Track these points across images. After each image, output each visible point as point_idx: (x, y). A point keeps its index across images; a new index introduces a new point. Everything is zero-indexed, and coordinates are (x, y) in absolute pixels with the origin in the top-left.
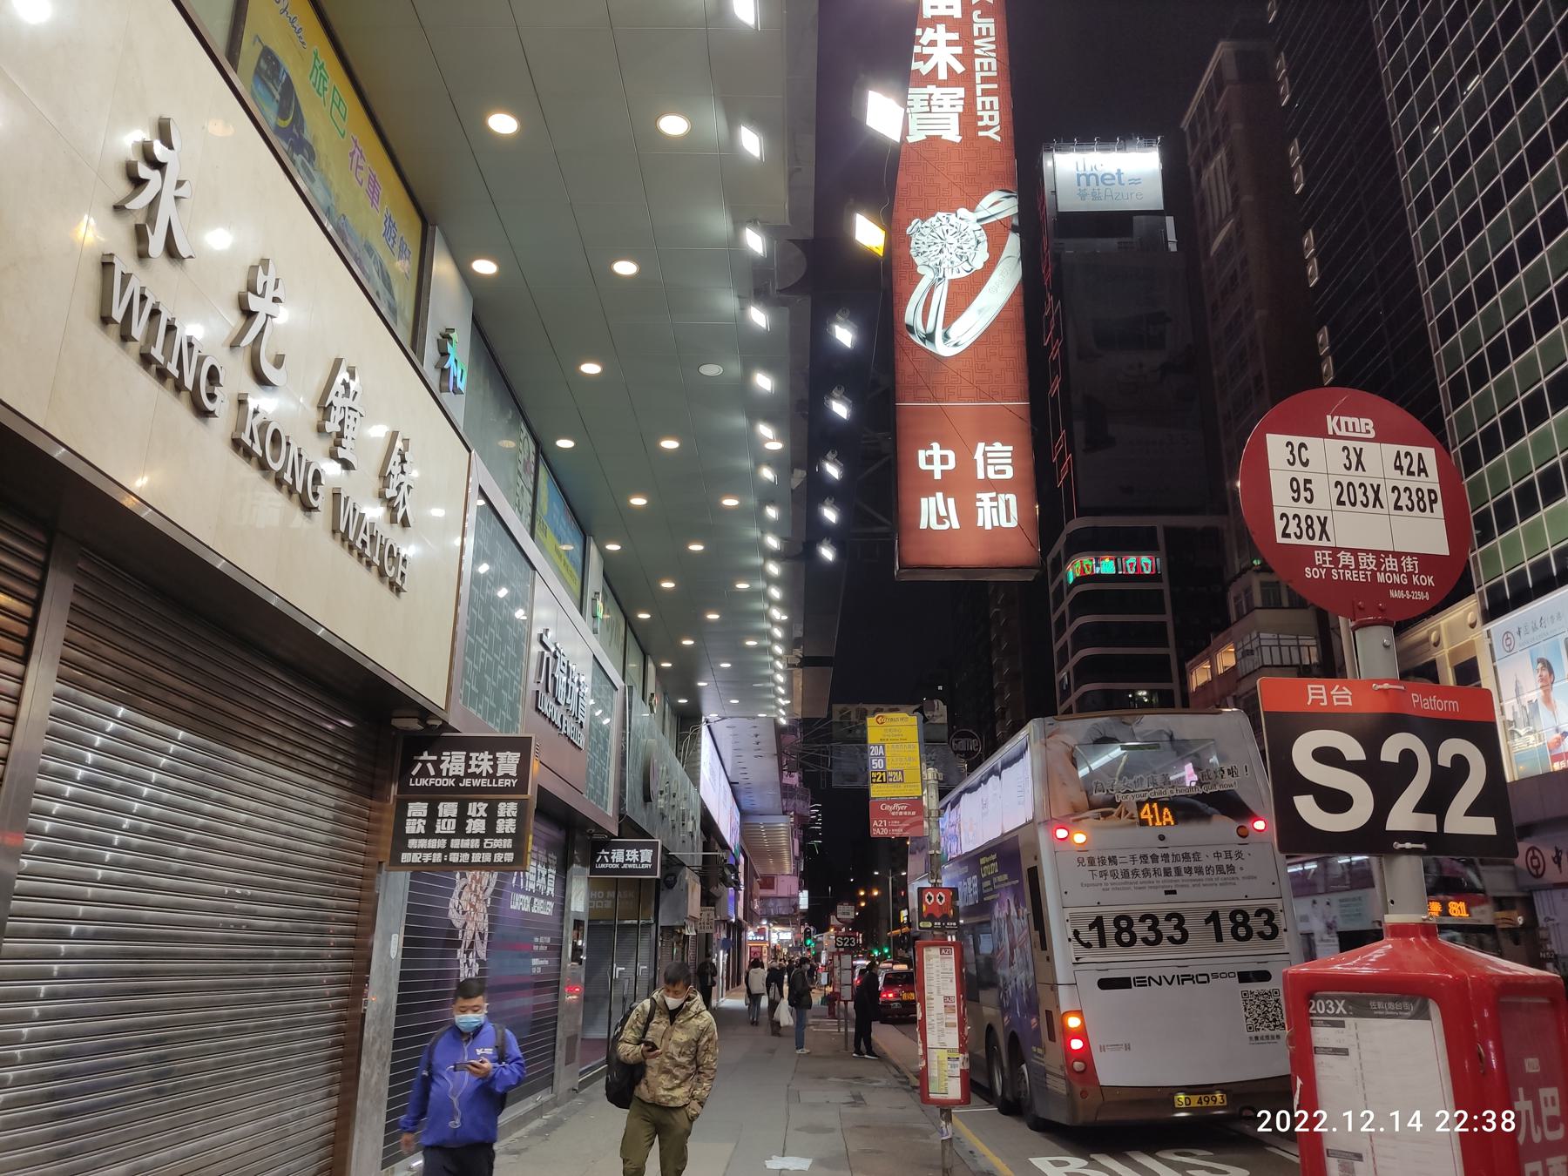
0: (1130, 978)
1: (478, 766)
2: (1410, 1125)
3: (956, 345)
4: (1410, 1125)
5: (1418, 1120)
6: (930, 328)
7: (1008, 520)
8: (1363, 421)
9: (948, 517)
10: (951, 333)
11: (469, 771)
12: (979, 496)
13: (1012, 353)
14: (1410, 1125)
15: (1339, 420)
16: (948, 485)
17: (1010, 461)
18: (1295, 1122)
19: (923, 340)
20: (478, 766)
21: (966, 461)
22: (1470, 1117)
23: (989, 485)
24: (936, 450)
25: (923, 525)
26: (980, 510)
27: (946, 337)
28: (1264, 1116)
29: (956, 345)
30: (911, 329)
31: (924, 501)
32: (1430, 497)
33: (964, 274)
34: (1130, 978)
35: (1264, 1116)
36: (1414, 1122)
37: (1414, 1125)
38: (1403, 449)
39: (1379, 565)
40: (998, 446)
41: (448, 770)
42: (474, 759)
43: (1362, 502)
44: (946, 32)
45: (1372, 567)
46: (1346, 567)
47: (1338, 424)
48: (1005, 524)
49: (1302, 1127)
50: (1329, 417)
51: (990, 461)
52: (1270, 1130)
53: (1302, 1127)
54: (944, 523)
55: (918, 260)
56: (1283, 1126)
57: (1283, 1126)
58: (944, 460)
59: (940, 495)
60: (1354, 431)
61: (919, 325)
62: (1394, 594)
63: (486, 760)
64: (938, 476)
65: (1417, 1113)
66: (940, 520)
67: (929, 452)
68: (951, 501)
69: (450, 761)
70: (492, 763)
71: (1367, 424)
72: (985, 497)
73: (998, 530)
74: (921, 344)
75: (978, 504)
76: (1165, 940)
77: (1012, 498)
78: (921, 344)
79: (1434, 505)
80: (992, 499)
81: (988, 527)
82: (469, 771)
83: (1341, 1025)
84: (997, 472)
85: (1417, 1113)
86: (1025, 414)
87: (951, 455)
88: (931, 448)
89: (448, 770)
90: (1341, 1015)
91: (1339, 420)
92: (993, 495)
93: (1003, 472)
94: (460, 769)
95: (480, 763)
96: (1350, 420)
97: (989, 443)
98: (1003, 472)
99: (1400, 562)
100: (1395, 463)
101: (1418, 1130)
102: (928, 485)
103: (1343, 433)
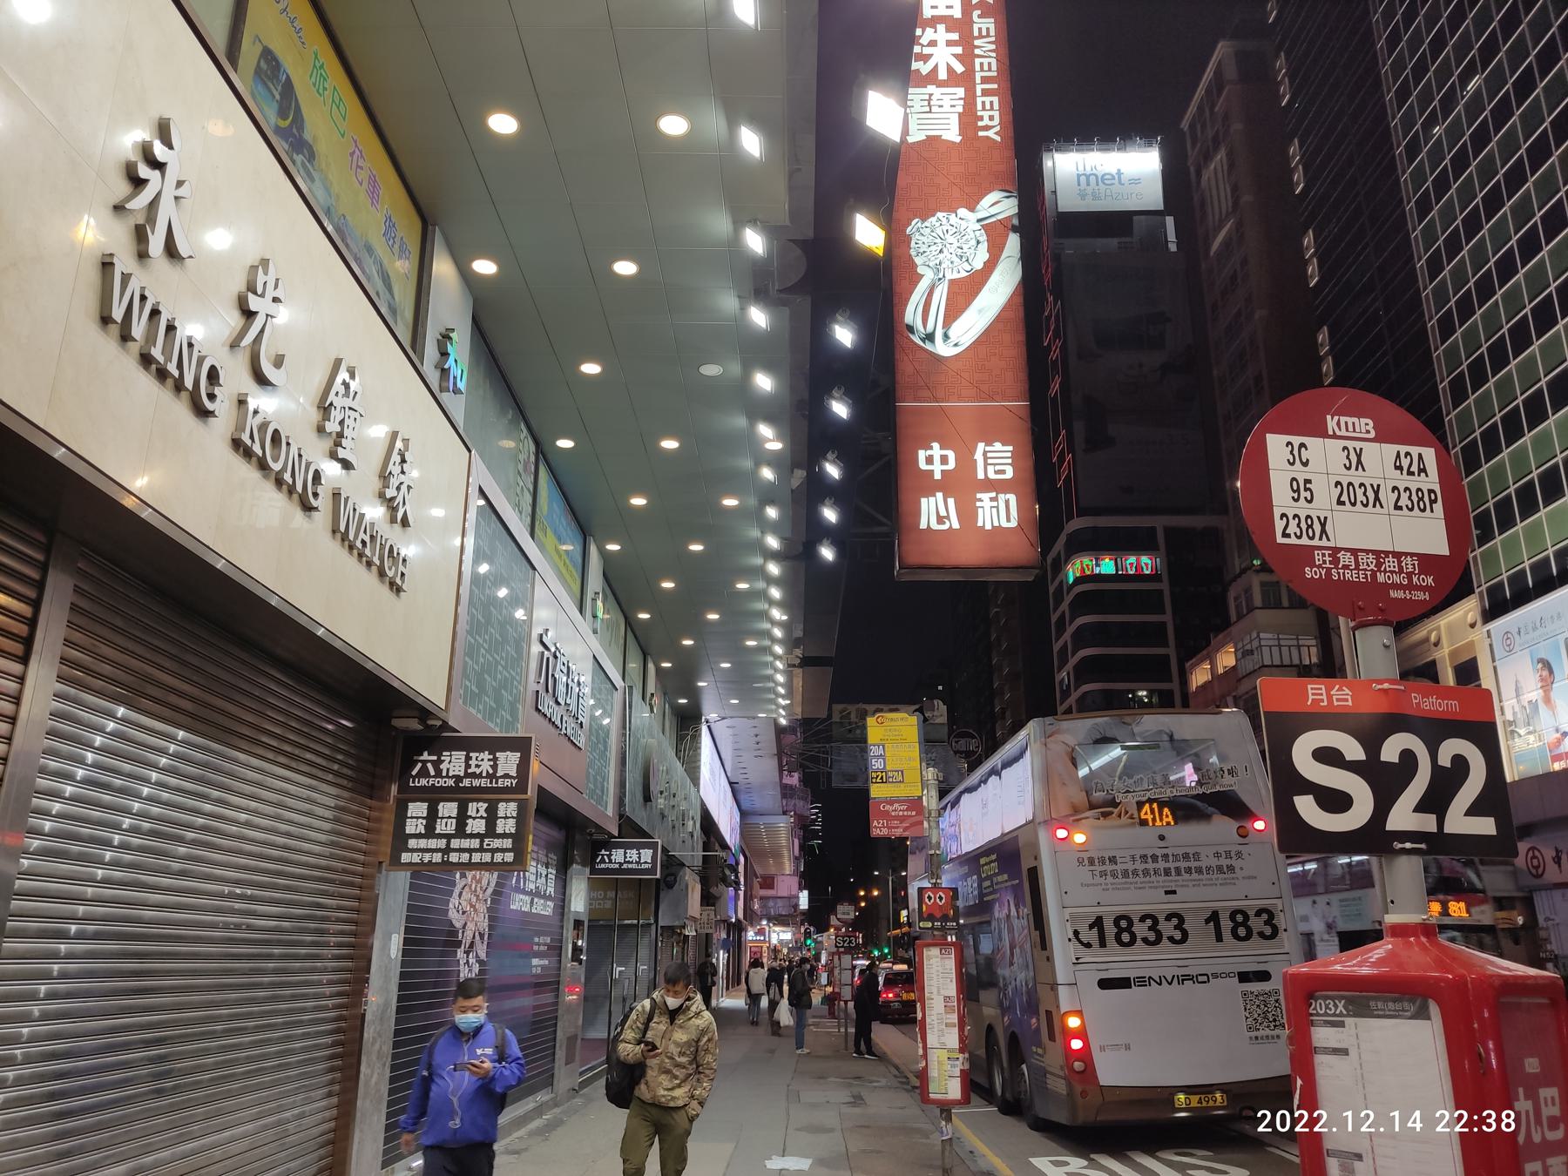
0: (1130, 978)
1: (478, 766)
2: (1410, 1125)
3: (956, 345)
4: (1410, 1125)
5: (1418, 1120)
6: (930, 328)
7: (1008, 520)
8: (1363, 421)
9: (948, 517)
10: (951, 333)
11: (469, 771)
12: (979, 496)
13: (1012, 353)
14: (1410, 1125)
15: (1339, 420)
16: (948, 485)
17: (1010, 461)
18: (1295, 1122)
19: (923, 340)
20: (478, 766)
21: (966, 461)
22: (1470, 1117)
23: (989, 485)
24: (936, 450)
25: (923, 525)
26: (980, 510)
27: (946, 337)
28: (1264, 1116)
29: (956, 345)
30: (911, 329)
31: (924, 501)
32: (1430, 497)
33: (964, 274)
34: (1130, 978)
35: (1264, 1116)
36: (1414, 1122)
37: (1414, 1125)
38: (1403, 449)
39: (1379, 565)
40: (998, 446)
41: (448, 770)
42: (474, 759)
43: (1362, 502)
44: (946, 32)
45: (1372, 567)
46: (1346, 567)
47: (1338, 424)
48: (1005, 524)
49: (1302, 1127)
50: (1329, 417)
51: (990, 461)
52: (1270, 1130)
53: (1302, 1127)
54: (944, 523)
55: (918, 260)
56: (1283, 1126)
57: (1283, 1126)
58: (944, 460)
59: (940, 495)
60: (1354, 431)
61: (919, 325)
62: (1394, 594)
63: (486, 760)
64: (938, 476)
65: (1417, 1113)
66: (940, 520)
67: (929, 452)
68: (951, 501)
69: (450, 761)
70: (492, 763)
71: (1367, 424)
72: (985, 497)
73: (998, 530)
74: (921, 344)
75: (978, 504)
76: (1165, 940)
77: (1012, 498)
78: (921, 344)
79: (1434, 505)
80: (992, 499)
81: (988, 527)
82: (469, 771)
83: (1341, 1025)
84: (997, 472)
85: (1417, 1113)
86: (1025, 414)
87: (951, 455)
88: (931, 448)
89: (448, 770)
90: (1341, 1015)
91: (1339, 420)
92: (993, 495)
93: (1003, 472)
94: (460, 769)
95: (480, 763)
96: (1350, 420)
97: (989, 443)
98: (1003, 472)
99: (1400, 562)
100: (1395, 463)
101: (1418, 1130)
102: (928, 485)
103: (1343, 433)
